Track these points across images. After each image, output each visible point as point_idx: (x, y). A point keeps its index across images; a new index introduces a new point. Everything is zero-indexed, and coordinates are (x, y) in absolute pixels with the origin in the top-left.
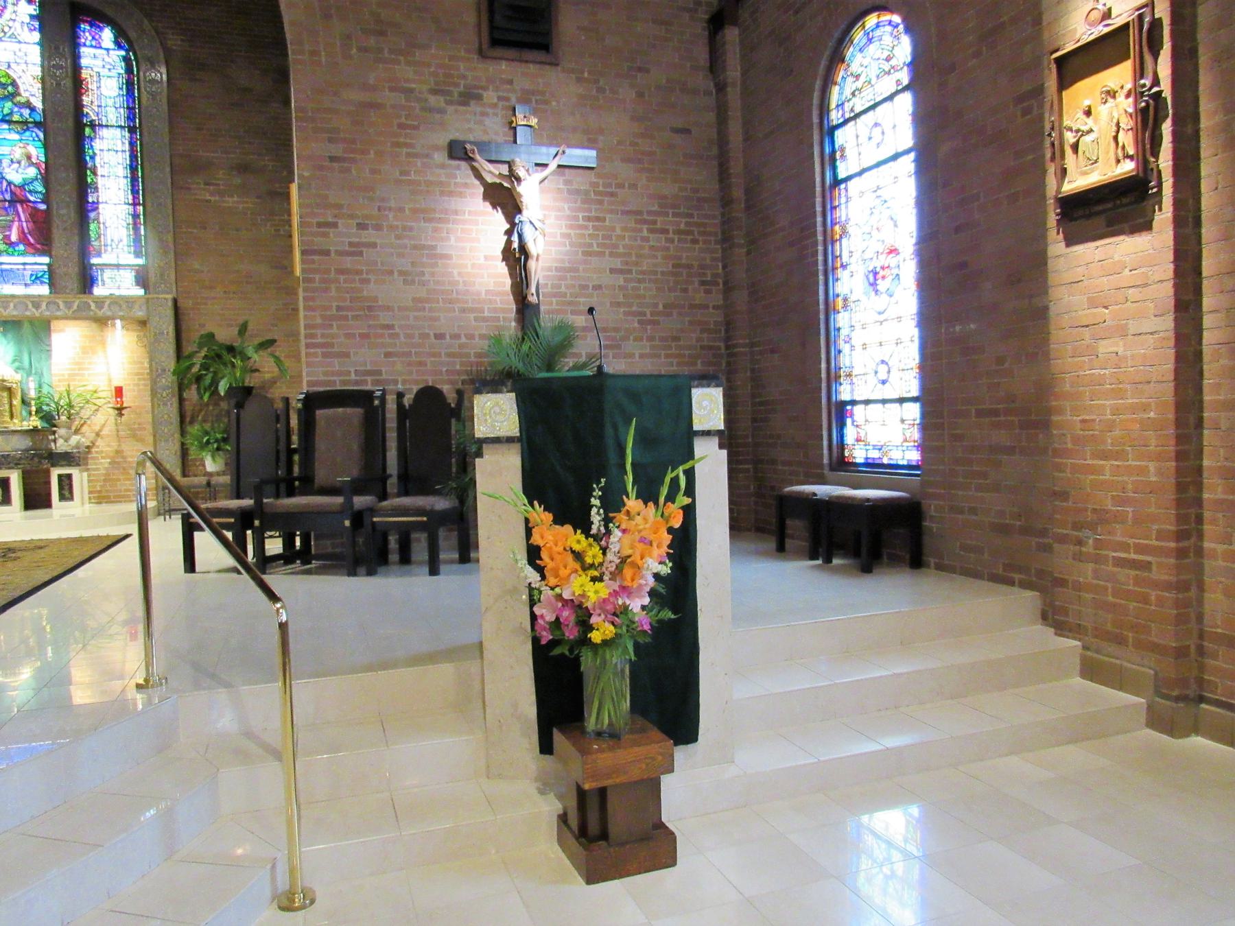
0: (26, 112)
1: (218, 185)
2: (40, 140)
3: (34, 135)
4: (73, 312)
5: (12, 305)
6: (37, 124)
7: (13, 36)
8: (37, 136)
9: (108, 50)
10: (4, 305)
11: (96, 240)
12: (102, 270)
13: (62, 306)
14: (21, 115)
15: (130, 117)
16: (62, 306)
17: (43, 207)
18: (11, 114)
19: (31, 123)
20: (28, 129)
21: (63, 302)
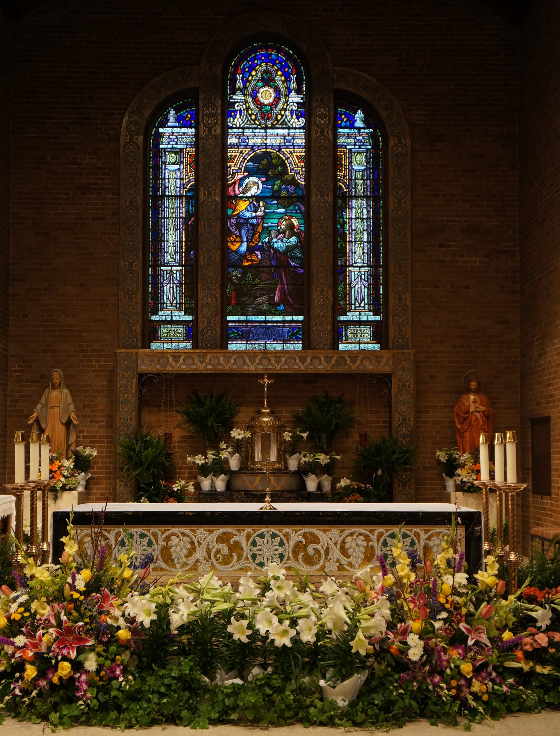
0: (291, 188)
1: (450, 246)
2: (301, 212)
3: (297, 208)
4: (332, 366)
5: (283, 360)
6: (300, 199)
7: (284, 123)
8: (299, 209)
9: (359, 129)
10: (278, 359)
11: (342, 299)
12: (347, 328)
13: (323, 360)
14: (288, 191)
15: (375, 188)
16: (323, 360)
17: (301, 271)
18: (279, 190)
19: (295, 197)
20: (292, 204)
21: (324, 357)
